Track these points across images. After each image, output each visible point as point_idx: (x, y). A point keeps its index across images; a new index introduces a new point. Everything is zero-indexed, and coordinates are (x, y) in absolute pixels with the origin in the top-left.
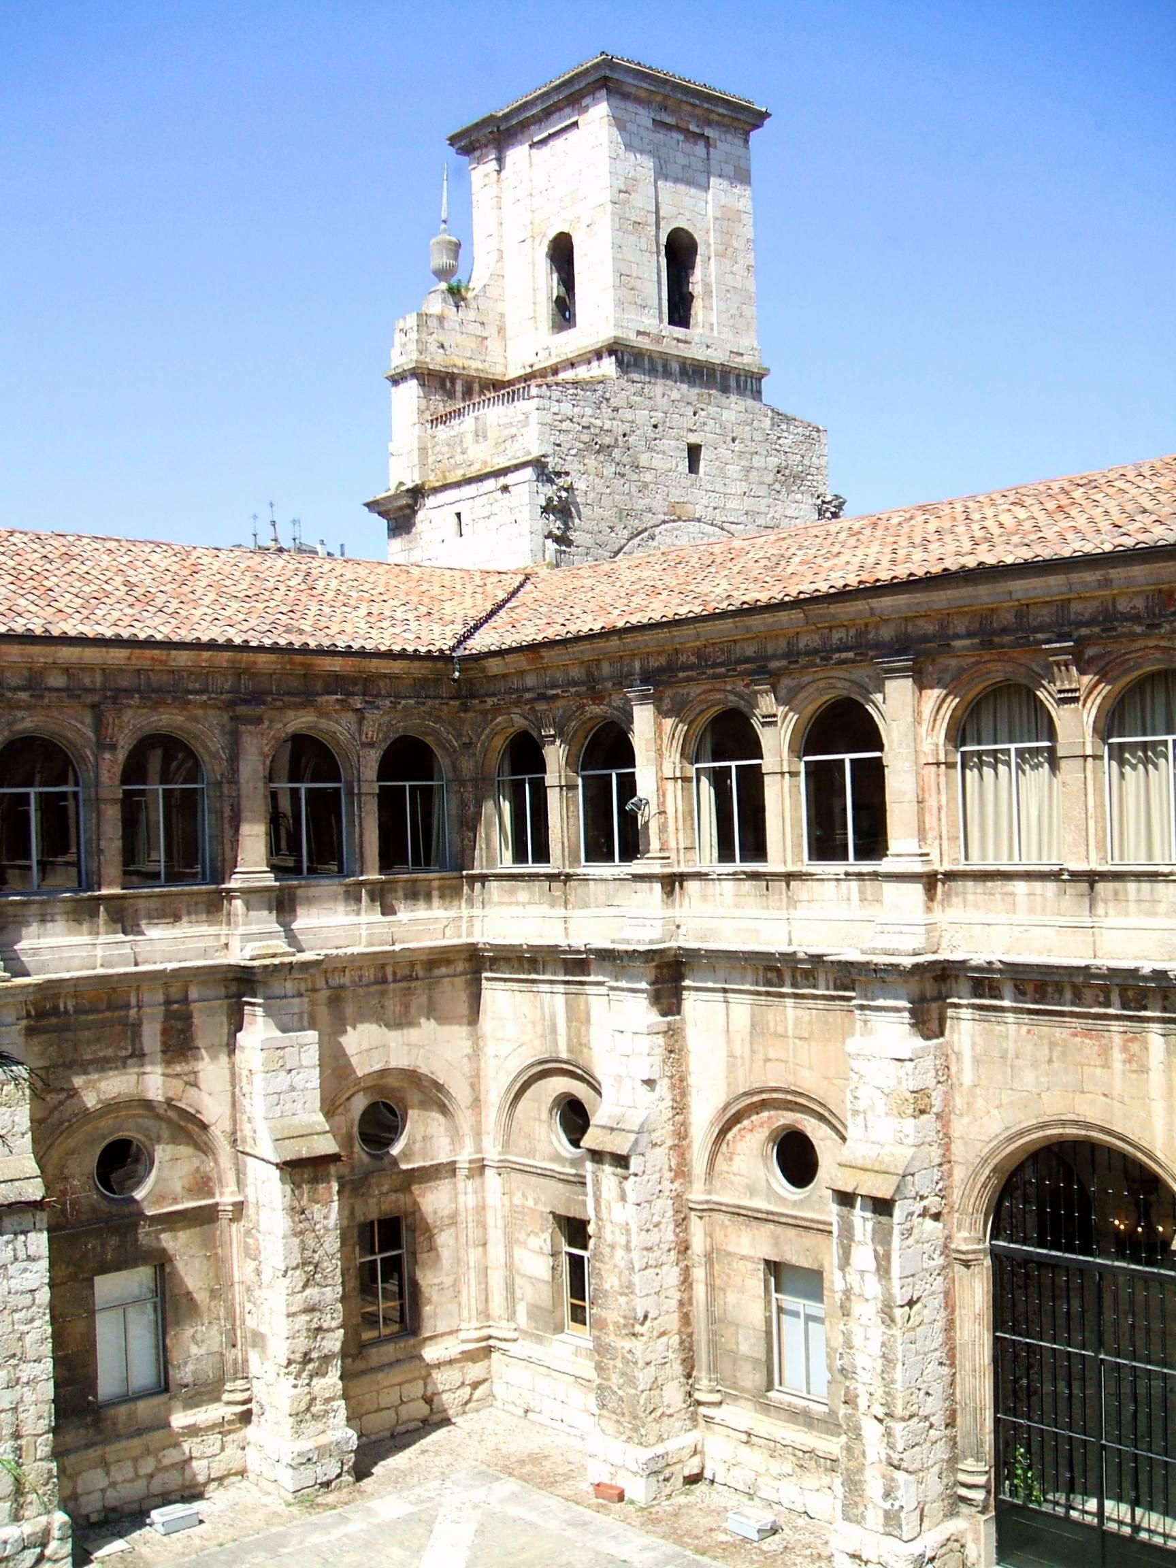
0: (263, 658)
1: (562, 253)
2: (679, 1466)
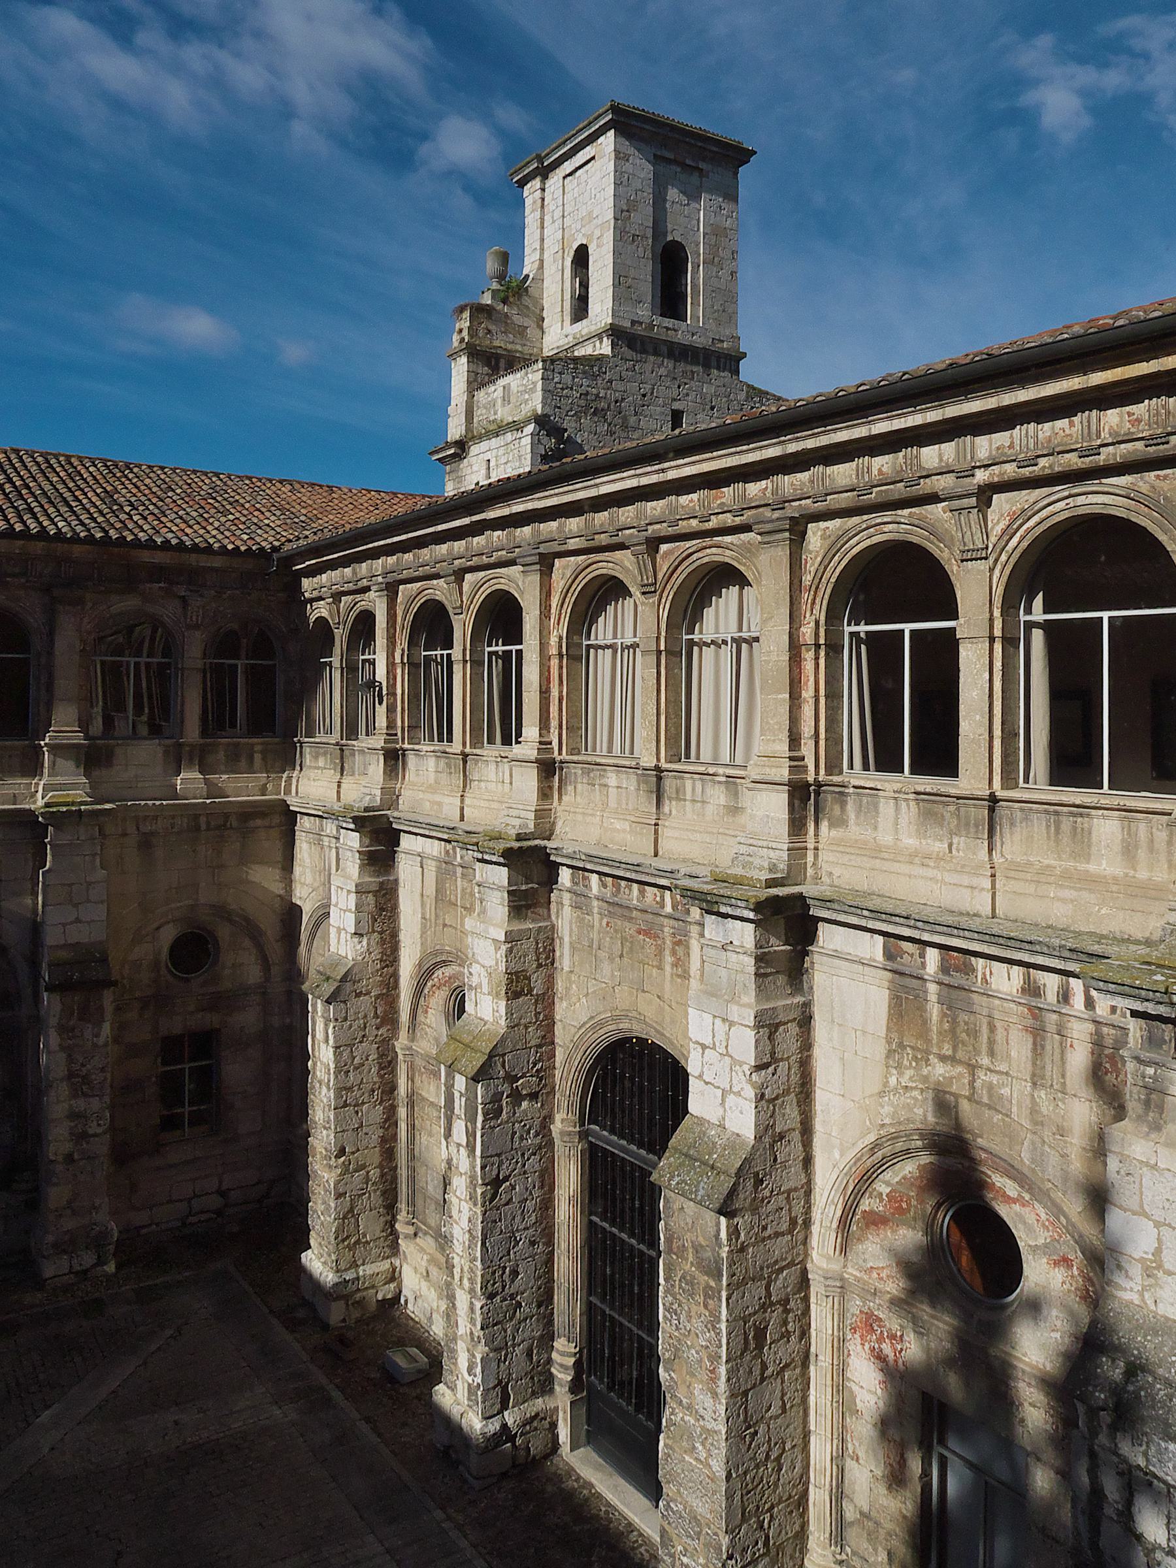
0: (77, 550)
1: (581, 258)
2: (373, 1291)
